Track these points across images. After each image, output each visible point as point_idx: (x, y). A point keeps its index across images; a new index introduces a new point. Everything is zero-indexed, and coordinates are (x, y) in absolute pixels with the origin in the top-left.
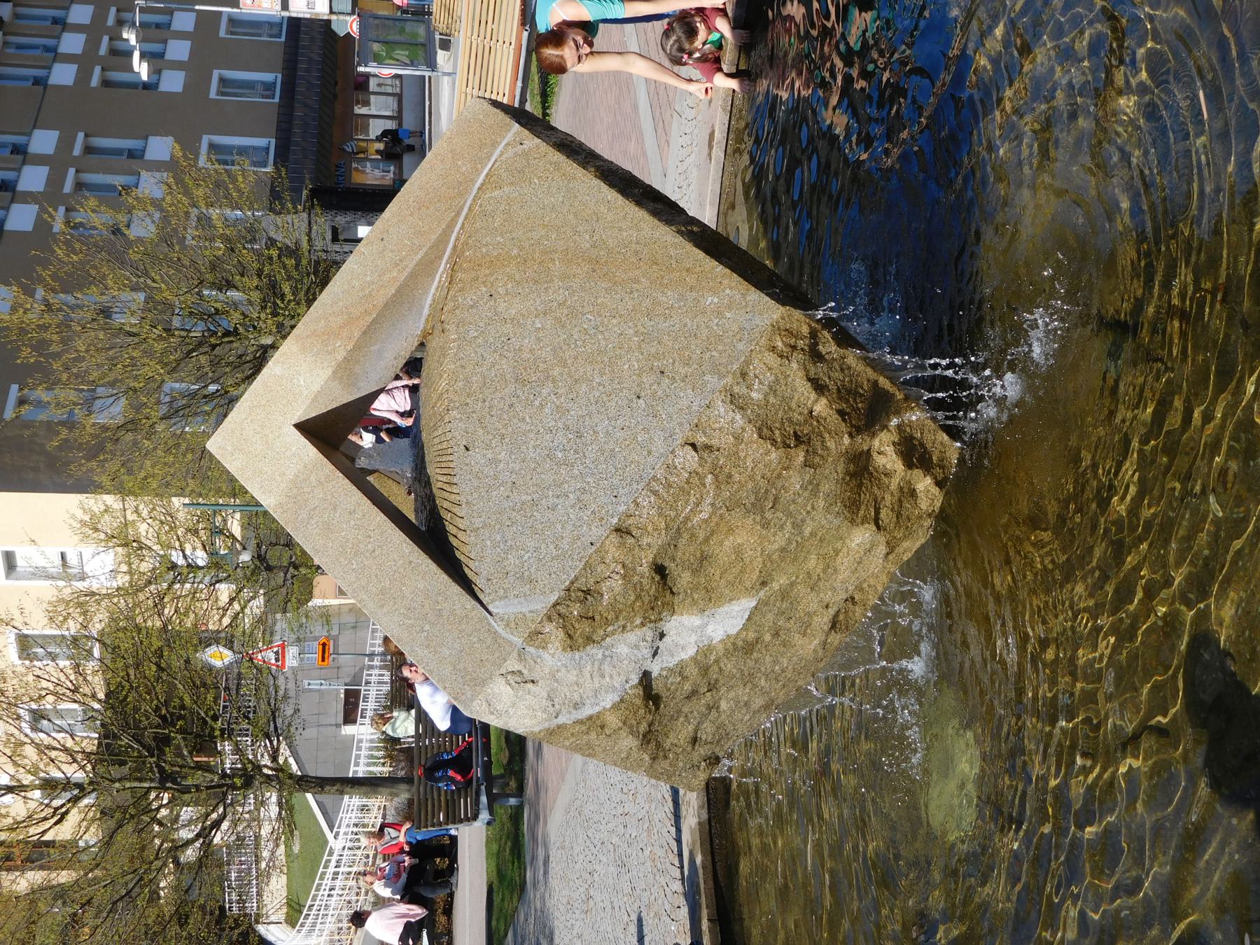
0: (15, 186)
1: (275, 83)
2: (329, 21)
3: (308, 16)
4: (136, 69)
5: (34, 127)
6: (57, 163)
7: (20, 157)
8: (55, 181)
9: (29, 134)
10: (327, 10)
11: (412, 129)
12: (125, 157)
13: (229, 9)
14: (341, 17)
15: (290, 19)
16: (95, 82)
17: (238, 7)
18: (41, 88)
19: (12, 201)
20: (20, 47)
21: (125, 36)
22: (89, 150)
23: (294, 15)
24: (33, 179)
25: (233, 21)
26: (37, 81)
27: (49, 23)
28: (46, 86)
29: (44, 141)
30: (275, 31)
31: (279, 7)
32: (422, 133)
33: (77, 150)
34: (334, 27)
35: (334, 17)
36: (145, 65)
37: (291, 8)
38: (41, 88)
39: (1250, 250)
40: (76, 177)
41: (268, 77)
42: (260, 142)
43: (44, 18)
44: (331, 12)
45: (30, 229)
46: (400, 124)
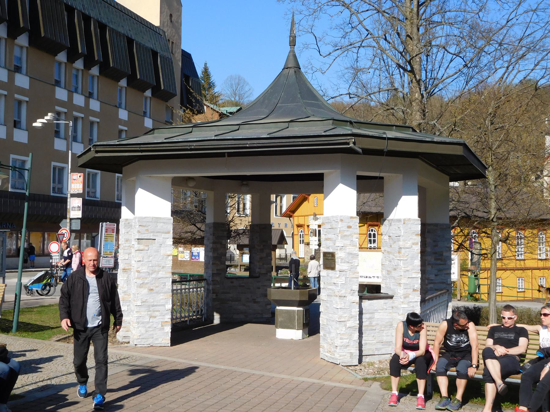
0: (18, 72)
1: (62, 193)
2: (66, 218)
3: (68, 207)
4: (38, 121)
5: (30, 77)
6: (86, 109)
7: (88, 95)
8: (79, 109)
9: (27, 75)
10: (72, 217)
11: (35, 261)
12: (56, 129)
13: (70, 167)
14: (68, 224)
15: (66, 198)
16: (121, 127)
17: (71, 172)
18: (54, 83)
19: (9, 70)
20: (77, 76)
21: (49, 114)
22: (92, 123)
23: (68, 200)
24: (79, 100)
25: (61, 170)
26: (145, 113)
27: (144, 110)
28: (55, 85)
29: (95, 105)
30: (91, 194)
31: (72, 192)
32: (33, 267)
33: (92, 118)
34: (64, 220)
35: (68, 220)
36: (40, 125)
37: (72, 199)
38: (143, 114)
39: (346, 382)
40: (80, 117)
41: (98, 195)
42: (98, 195)
43: (146, 109)
44: (71, 219)
45: (145, 125)
46: (39, 256)
